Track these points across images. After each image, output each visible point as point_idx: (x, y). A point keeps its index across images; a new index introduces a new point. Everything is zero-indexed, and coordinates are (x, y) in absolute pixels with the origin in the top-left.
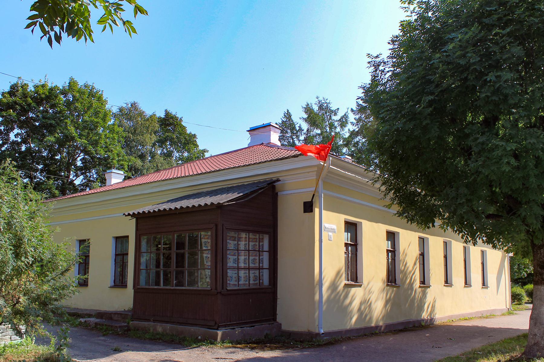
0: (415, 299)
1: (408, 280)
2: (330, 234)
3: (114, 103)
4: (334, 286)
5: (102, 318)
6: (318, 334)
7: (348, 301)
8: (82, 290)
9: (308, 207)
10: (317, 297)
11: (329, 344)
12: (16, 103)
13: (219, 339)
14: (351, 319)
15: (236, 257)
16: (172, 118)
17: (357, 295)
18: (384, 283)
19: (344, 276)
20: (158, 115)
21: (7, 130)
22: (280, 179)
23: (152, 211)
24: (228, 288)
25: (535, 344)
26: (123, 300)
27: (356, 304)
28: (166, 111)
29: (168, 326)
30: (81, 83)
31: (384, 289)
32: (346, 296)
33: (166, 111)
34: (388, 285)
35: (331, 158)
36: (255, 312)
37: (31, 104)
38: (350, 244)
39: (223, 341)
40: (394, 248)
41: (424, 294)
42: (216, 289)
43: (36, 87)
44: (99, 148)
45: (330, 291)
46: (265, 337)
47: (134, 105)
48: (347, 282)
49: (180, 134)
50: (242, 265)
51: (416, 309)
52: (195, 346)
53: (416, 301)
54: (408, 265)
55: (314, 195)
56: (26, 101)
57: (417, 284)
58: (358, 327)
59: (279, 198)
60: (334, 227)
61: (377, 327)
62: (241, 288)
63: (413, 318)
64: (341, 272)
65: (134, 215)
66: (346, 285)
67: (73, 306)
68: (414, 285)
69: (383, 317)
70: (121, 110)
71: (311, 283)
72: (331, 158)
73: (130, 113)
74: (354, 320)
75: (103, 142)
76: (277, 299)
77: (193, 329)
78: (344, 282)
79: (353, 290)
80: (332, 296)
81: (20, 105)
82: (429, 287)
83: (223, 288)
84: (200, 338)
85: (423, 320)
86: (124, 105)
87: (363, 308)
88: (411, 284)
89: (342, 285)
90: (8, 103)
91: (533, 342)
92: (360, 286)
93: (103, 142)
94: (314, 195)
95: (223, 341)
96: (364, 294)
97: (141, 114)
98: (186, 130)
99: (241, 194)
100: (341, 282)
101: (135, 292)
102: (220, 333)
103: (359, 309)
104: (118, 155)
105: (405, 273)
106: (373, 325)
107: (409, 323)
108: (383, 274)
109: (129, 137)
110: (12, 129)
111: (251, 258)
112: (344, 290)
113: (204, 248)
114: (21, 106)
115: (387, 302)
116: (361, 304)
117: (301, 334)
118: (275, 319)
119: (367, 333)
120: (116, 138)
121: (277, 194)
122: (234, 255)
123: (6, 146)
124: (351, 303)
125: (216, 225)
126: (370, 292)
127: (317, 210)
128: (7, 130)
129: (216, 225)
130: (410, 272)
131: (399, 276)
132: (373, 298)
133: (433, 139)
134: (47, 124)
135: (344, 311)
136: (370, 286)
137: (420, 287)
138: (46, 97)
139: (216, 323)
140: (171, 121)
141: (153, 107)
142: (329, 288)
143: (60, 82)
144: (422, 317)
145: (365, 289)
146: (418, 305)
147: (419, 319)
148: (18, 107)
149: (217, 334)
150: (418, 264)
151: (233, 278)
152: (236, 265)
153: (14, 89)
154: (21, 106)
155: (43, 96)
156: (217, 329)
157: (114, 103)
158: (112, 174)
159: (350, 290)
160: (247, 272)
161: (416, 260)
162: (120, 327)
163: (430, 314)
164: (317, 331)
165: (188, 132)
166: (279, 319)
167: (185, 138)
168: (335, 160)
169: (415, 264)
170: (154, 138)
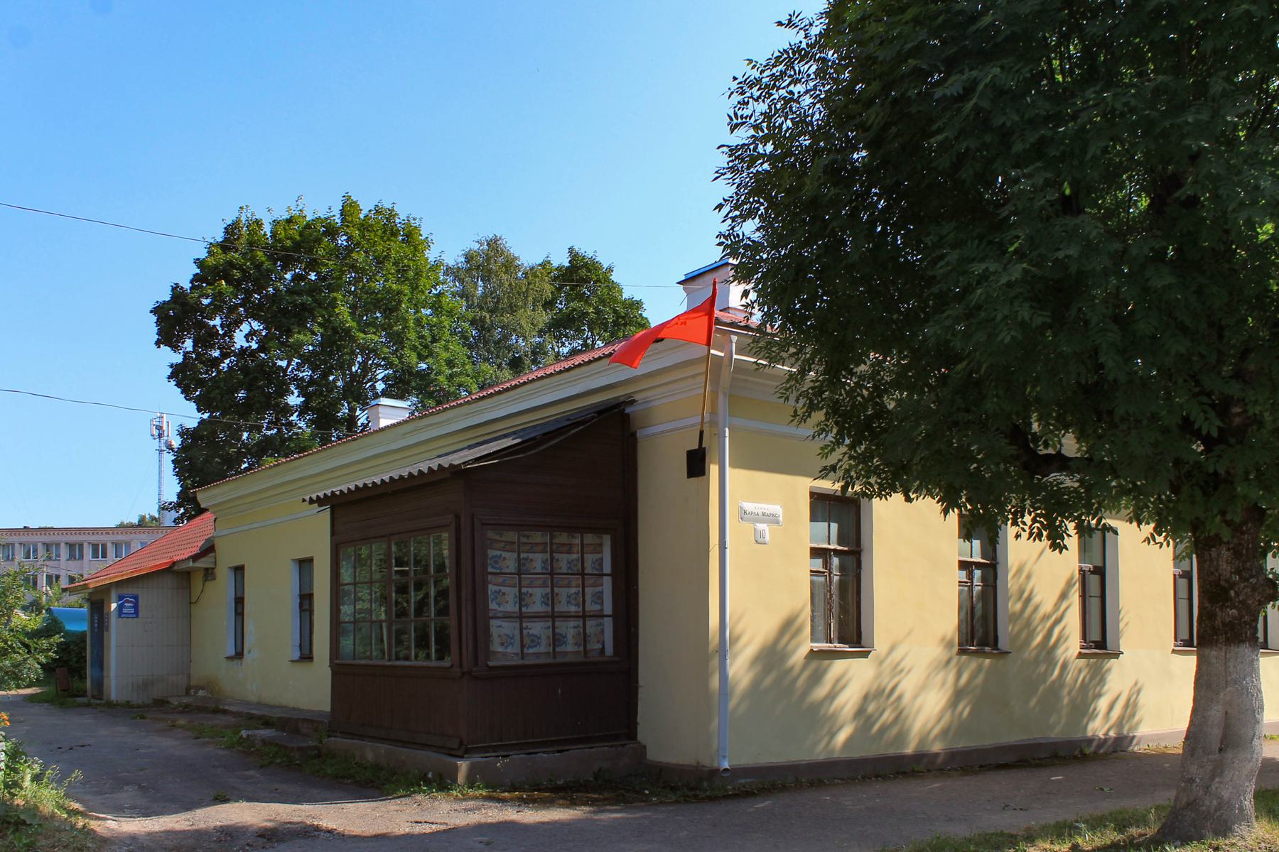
0: (1062, 686)
1: (1039, 639)
2: (761, 526)
3: (447, 245)
4: (772, 656)
5: (283, 729)
6: (715, 772)
7: (821, 692)
8: (304, 668)
9: (697, 464)
10: (715, 682)
11: (746, 794)
12: (231, 264)
13: (461, 778)
14: (833, 735)
15: (549, 590)
16: (586, 266)
17: (852, 678)
18: (949, 645)
19: (808, 630)
20: (555, 264)
21: (228, 326)
22: (636, 397)
23: (353, 488)
24: (491, 664)
25: (1189, 804)
26: (311, 690)
27: (848, 700)
28: (571, 250)
29: (383, 748)
30: (366, 207)
31: (949, 661)
32: (816, 678)
33: (571, 250)
34: (962, 652)
35: (734, 338)
36: (585, 714)
37: (263, 262)
38: (835, 551)
39: (471, 783)
40: (994, 558)
41: (1098, 677)
42: (461, 666)
43: (276, 223)
44: (407, 351)
45: (758, 668)
46: (596, 778)
47: (494, 244)
48: (818, 646)
49: (603, 302)
50: (529, 606)
51: (1064, 712)
52: (402, 792)
53: (1066, 691)
54: (1036, 600)
55: (702, 433)
56: (253, 259)
57: (1072, 645)
58: (856, 754)
59: (642, 446)
60: (776, 509)
61: (919, 757)
62: (526, 662)
63: (1057, 730)
64: (800, 620)
65: (320, 501)
66: (813, 654)
67: (292, 704)
68: (1059, 651)
69: (945, 733)
70: (469, 257)
71: (707, 653)
72: (734, 338)
73: (488, 262)
74: (842, 737)
75: (412, 336)
76: (636, 689)
77: (421, 755)
78: (805, 645)
79: (839, 666)
80: (768, 681)
81: (240, 268)
82: (1116, 655)
83: (476, 664)
84: (430, 775)
85: (1090, 741)
86: (476, 246)
87: (871, 708)
88: (1048, 652)
89: (803, 650)
90: (216, 267)
91: (1185, 800)
92: (865, 655)
93: (412, 336)
94: (702, 433)
95: (471, 783)
96: (878, 675)
97: (510, 264)
98: (621, 292)
99: (518, 441)
100: (798, 646)
101: (335, 674)
102: (463, 766)
103: (860, 712)
104: (450, 363)
105: (1028, 623)
106: (909, 750)
107: (1035, 747)
108: (948, 621)
109: (482, 320)
110: (238, 323)
111: (588, 591)
112: (805, 667)
113: (490, 570)
114: (243, 271)
115: (958, 695)
116: (866, 698)
117: (681, 770)
118: (631, 733)
119: (885, 768)
120: (446, 324)
121: (634, 435)
122: (544, 586)
123: (227, 361)
124: (832, 696)
125: (457, 517)
126: (897, 670)
127: (714, 470)
128: (228, 326)
129: (457, 517)
130: (1046, 617)
131: (1006, 631)
132: (907, 686)
133: (923, 267)
134: (296, 306)
135: (818, 718)
136: (896, 655)
137: (1080, 656)
138: (300, 241)
139: (461, 744)
140: (583, 272)
141: (538, 246)
142: (756, 660)
143: (321, 205)
144: (1089, 734)
145: (881, 663)
146: (1072, 701)
147: (1079, 736)
148: (236, 274)
149: (456, 770)
150: (1075, 597)
151: (543, 637)
152: (549, 609)
153: (233, 234)
154: (243, 271)
155: (289, 243)
156: (461, 757)
157: (447, 245)
158: (381, 409)
159: (829, 666)
160: (581, 623)
161: (1069, 585)
162: (300, 749)
163: (1120, 723)
164: (716, 765)
165: (626, 295)
166: (643, 734)
167: (615, 311)
168: (742, 339)
169: (1064, 596)
170: (544, 317)
